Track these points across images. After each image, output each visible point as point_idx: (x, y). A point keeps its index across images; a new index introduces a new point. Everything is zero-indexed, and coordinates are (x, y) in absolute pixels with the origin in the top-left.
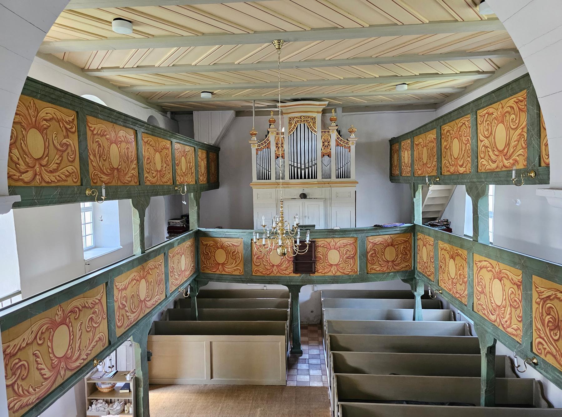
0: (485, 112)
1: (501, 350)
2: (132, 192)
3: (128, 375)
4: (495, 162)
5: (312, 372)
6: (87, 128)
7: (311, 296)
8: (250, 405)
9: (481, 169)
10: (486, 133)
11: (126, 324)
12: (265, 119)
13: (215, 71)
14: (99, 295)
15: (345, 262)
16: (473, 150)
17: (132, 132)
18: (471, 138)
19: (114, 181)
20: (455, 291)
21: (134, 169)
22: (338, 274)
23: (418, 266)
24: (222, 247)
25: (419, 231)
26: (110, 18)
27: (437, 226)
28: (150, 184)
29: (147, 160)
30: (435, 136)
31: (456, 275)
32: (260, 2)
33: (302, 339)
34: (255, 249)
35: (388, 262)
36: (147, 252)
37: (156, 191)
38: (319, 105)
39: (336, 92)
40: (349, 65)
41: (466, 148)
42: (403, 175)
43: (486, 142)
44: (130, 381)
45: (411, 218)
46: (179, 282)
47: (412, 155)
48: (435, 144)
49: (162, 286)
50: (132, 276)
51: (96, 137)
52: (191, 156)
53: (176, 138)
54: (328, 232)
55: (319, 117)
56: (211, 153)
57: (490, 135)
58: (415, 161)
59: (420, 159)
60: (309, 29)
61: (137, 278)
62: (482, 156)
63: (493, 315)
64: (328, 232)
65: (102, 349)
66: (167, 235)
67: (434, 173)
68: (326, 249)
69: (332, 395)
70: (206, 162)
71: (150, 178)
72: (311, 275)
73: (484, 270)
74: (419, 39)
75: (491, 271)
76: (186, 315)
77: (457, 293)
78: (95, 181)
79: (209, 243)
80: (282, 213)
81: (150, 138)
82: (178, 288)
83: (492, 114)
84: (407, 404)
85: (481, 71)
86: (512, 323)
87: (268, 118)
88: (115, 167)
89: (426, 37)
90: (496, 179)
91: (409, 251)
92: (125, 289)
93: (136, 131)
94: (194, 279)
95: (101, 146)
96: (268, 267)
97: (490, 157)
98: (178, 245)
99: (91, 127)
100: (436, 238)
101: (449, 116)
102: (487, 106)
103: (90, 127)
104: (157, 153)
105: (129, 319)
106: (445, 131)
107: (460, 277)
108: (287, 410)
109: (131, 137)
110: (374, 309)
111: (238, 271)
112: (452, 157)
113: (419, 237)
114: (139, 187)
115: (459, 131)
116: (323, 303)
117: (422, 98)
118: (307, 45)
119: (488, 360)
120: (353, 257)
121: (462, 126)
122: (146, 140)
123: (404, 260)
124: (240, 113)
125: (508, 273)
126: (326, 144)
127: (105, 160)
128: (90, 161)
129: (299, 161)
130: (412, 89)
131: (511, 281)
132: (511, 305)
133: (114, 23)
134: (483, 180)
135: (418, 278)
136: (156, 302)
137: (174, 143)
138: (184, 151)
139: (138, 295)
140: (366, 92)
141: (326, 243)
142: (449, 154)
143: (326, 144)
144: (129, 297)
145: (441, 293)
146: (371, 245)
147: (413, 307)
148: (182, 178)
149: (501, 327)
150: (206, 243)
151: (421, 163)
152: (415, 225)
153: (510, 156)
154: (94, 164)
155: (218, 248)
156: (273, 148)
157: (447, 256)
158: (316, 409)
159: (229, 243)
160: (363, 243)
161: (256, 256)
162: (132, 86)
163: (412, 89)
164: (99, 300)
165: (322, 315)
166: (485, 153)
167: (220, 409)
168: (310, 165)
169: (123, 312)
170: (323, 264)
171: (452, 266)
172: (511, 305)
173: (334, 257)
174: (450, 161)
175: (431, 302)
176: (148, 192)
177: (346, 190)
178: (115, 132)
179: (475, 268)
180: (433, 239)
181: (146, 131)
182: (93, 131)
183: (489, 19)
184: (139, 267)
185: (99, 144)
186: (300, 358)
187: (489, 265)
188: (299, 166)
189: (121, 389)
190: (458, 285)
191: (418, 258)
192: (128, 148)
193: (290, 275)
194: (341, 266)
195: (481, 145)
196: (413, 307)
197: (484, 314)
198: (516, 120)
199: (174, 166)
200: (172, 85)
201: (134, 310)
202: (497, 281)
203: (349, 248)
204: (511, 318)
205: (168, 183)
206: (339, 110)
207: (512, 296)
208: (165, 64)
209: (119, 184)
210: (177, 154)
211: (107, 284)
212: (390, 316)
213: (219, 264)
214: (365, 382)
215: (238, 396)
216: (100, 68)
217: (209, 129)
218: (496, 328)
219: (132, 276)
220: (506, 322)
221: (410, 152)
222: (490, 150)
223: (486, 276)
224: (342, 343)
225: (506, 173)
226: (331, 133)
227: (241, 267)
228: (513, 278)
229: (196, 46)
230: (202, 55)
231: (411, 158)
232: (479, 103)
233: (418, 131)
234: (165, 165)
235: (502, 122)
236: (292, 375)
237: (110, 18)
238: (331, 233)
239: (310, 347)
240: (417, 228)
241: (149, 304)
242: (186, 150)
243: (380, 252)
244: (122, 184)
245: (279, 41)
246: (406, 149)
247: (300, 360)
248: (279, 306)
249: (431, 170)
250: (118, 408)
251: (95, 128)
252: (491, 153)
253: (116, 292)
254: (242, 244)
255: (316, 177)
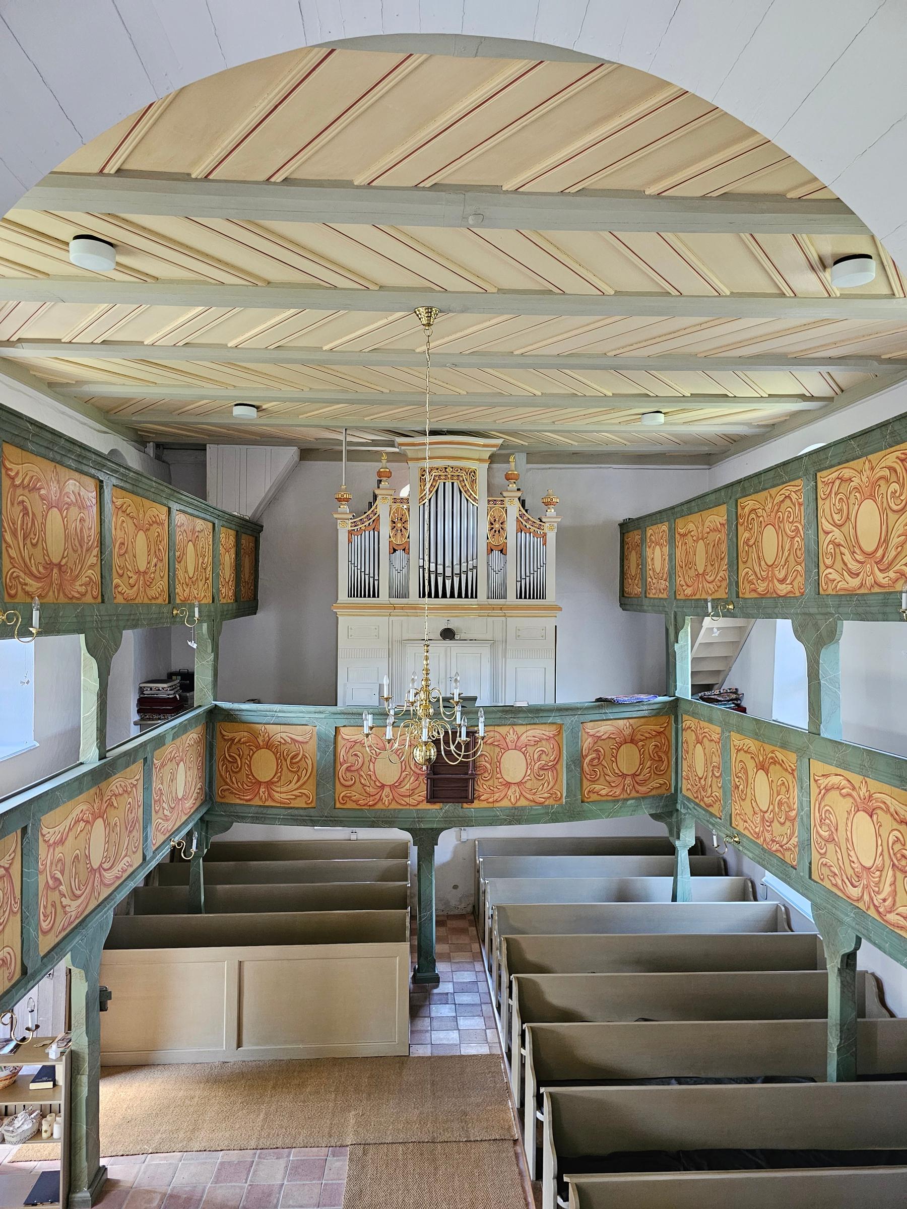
0: (836, 474)
1: (868, 959)
2: (88, 619)
3: (54, 1046)
4: (858, 575)
5: (463, 1023)
6: (3, 471)
7: (455, 852)
8: (331, 1105)
9: (827, 589)
10: (837, 517)
11: (59, 926)
12: (370, 468)
13: (275, 362)
14: (7, 857)
15: (538, 777)
16: (808, 551)
17: (91, 483)
18: (804, 527)
19: (51, 593)
20: (768, 836)
21: (92, 566)
22: (523, 803)
23: (685, 785)
24: (268, 746)
25: (687, 712)
26: (66, 232)
27: (718, 701)
28: (123, 601)
29: (120, 548)
30: (723, 520)
31: (771, 803)
32: (410, 229)
33: (438, 948)
34: (342, 753)
35: (624, 776)
36: (111, 755)
37: (131, 616)
38: (484, 446)
39: (519, 422)
40: (559, 367)
41: (792, 545)
42: (651, 596)
43: (837, 534)
44: (59, 1059)
45: (667, 683)
46: (170, 826)
47: (672, 557)
48: (723, 536)
49: (137, 834)
50: (77, 811)
51: (19, 491)
52: (206, 540)
53: (179, 501)
54: (503, 711)
55: (482, 470)
56: (244, 536)
57: (847, 520)
58: (678, 568)
59: (690, 564)
60: (495, 290)
61: (88, 816)
62: (829, 562)
63: (855, 887)
64: (503, 711)
65: (8, 985)
66: (136, 717)
67: (721, 594)
68: (497, 749)
69: (518, 1076)
70: (234, 556)
71: (124, 589)
72: (465, 805)
73: (834, 794)
74: (704, 326)
75: (849, 795)
76: (173, 903)
77: (773, 841)
78: (13, 592)
79: (237, 736)
80: (427, 670)
81: (128, 500)
82: (169, 839)
83: (850, 480)
84: (680, 1084)
85: (808, 394)
86: (898, 904)
87: (376, 466)
88: (55, 561)
89: (717, 322)
90: (860, 610)
91: (666, 753)
92: (62, 842)
93: (102, 482)
94: (202, 819)
95: (27, 514)
96: (371, 790)
97: (846, 565)
98: (173, 739)
99: (11, 470)
100: (726, 726)
101: (756, 481)
102: (839, 464)
103: (8, 469)
104: (141, 532)
105: (65, 913)
106: (747, 510)
107: (779, 808)
108: (417, 1112)
109: (90, 494)
110: (590, 878)
111: (304, 799)
112: (763, 563)
113: (687, 724)
114: (102, 607)
115: (778, 511)
116: (482, 867)
117: (685, 443)
118: (485, 321)
119: (842, 982)
120: (554, 766)
121: (783, 501)
122: (119, 502)
123: (657, 772)
124: (307, 453)
125: (888, 800)
126: (497, 526)
127: (34, 545)
128: (4, 546)
129: (440, 561)
130: (671, 424)
131: (895, 816)
132: (894, 865)
133: (74, 244)
134: (832, 610)
135: (683, 811)
136: (124, 871)
137: (174, 512)
138: (193, 531)
139: (88, 857)
140: (580, 424)
141: (498, 737)
142: (754, 555)
143: (497, 527)
144: (68, 860)
145: (738, 843)
146: (590, 740)
147: (671, 872)
148: (187, 590)
149: (872, 912)
150: (230, 735)
151: (692, 573)
152: (678, 699)
153: (890, 564)
154: (13, 553)
155: (259, 747)
156: (385, 529)
157: (751, 765)
158: (478, 1105)
159: (283, 735)
160: (575, 736)
161: (345, 766)
162: (80, 383)
163: (671, 424)
164: (7, 869)
165: (478, 894)
166: (834, 556)
167: (262, 1116)
168: (464, 569)
169: (55, 896)
170: (490, 783)
171: (761, 786)
172: (894, 865)
173: (514, 766)
174: (757, 569)
175: (707, 862)
176: (117, 620)
177: (531, 624)
178: (58, 482)
179: (814, 790)
180: (719, 730)
181: (122, 484)
182: (13, 479)
183: (844, 296)
184: (92, 791)
185: (25, 508)
186: (435, 991)
187: (844, 783)
188: (440, 570)
189: (33, 1082)
190: (776, 824)
191: (685, 767)
192: (82, 520)
193: (419, 807)
194: (528, 785)
195: (824, 540)
196: (671, 872)
197: (836, 885)
198: (901, 495)
199: (173, 561)
200: (174, 386)
201: (78, 893)
202: (862, 816)
203: (546, 747)
204: (894, 893)
205: (159, 601)
206: (522, 458)
207: (898, 847)
208: (168, 341)
209: (62, 599)
210: (179, 537)
211: (24, 830)
212: (623, 895)
213: (260, 783)
214: (592, 1039)
215: (301, 1085)
216: (14, 339)
217: (242, 484)
218: (861, 914)
219: (77, 811)
220: (884, 900)
221: (666, 550)
222: (845, 551)
223: (840, 806)
224: (531, 956)
225: (881, 597)
226: (507, 504)
227: (309, 790)
228: (898, 809)
229: (246, 307)
230: (254, 328)
231: (670, 560)
232: (819, 460)
233: (685, 507)
234: (155, 560)
235: (872, 497)
236: (421, 1031)
237: (66, 232)
238: (508, 714)
239: (454, 967)
240: (683, 706)
241: (108, 876)
242: (198, 529)
243: (608, 756)
244: (66, 600)
245: (429, 310)
246: (657, 544)
247: (435, 998)
248: (386, 876)
249: (713, 586)
250: (26, 1127)
251: (17, 473)
252: (848, 558)
253: (42, 849)
254: (315, 738)
255: (474, 595)
